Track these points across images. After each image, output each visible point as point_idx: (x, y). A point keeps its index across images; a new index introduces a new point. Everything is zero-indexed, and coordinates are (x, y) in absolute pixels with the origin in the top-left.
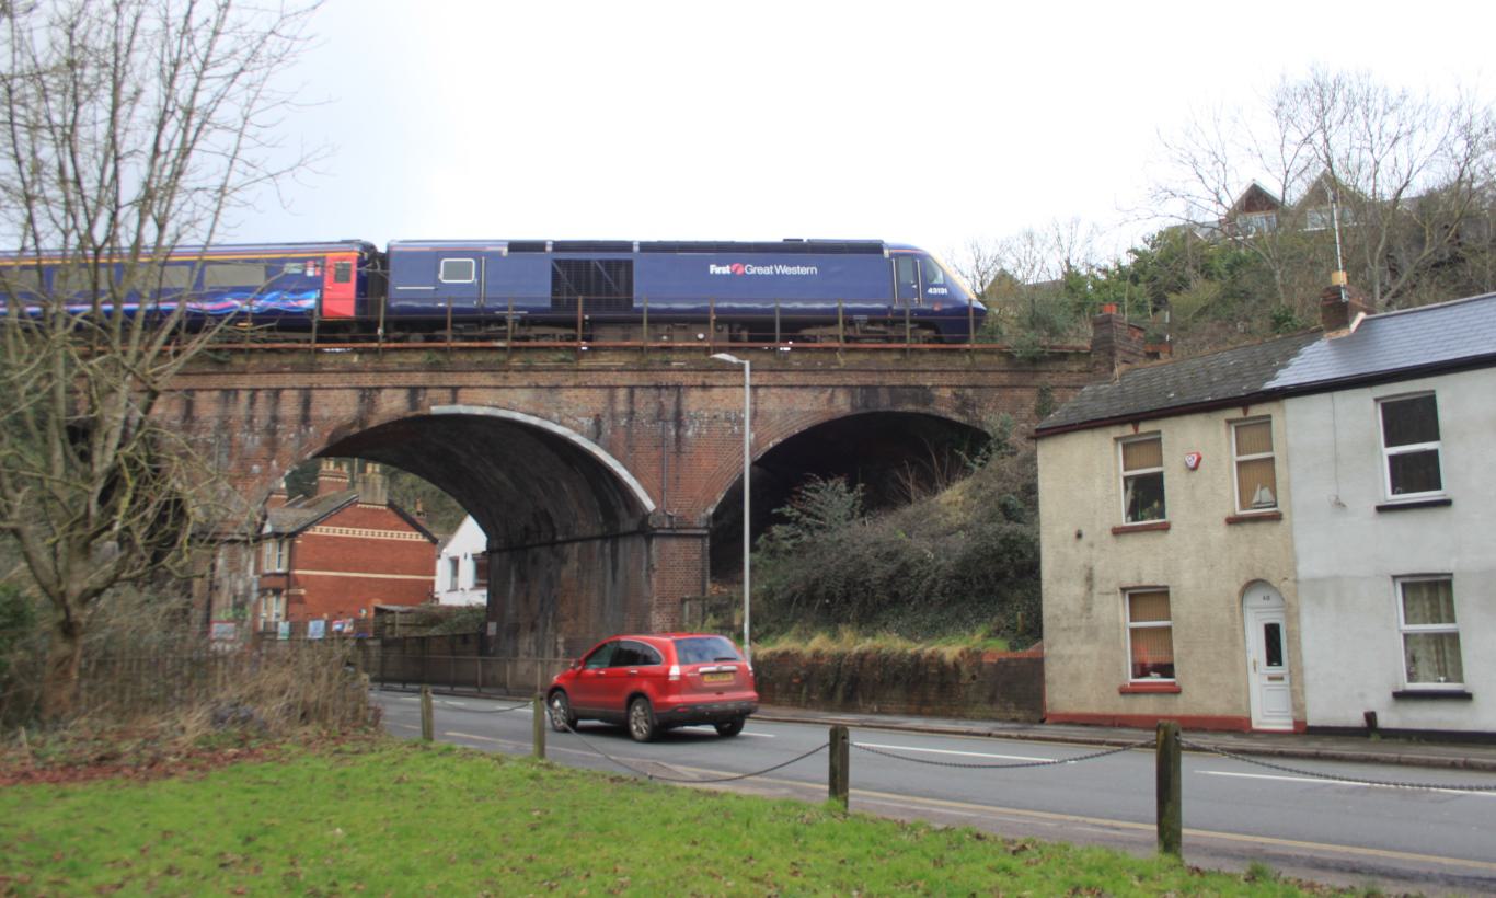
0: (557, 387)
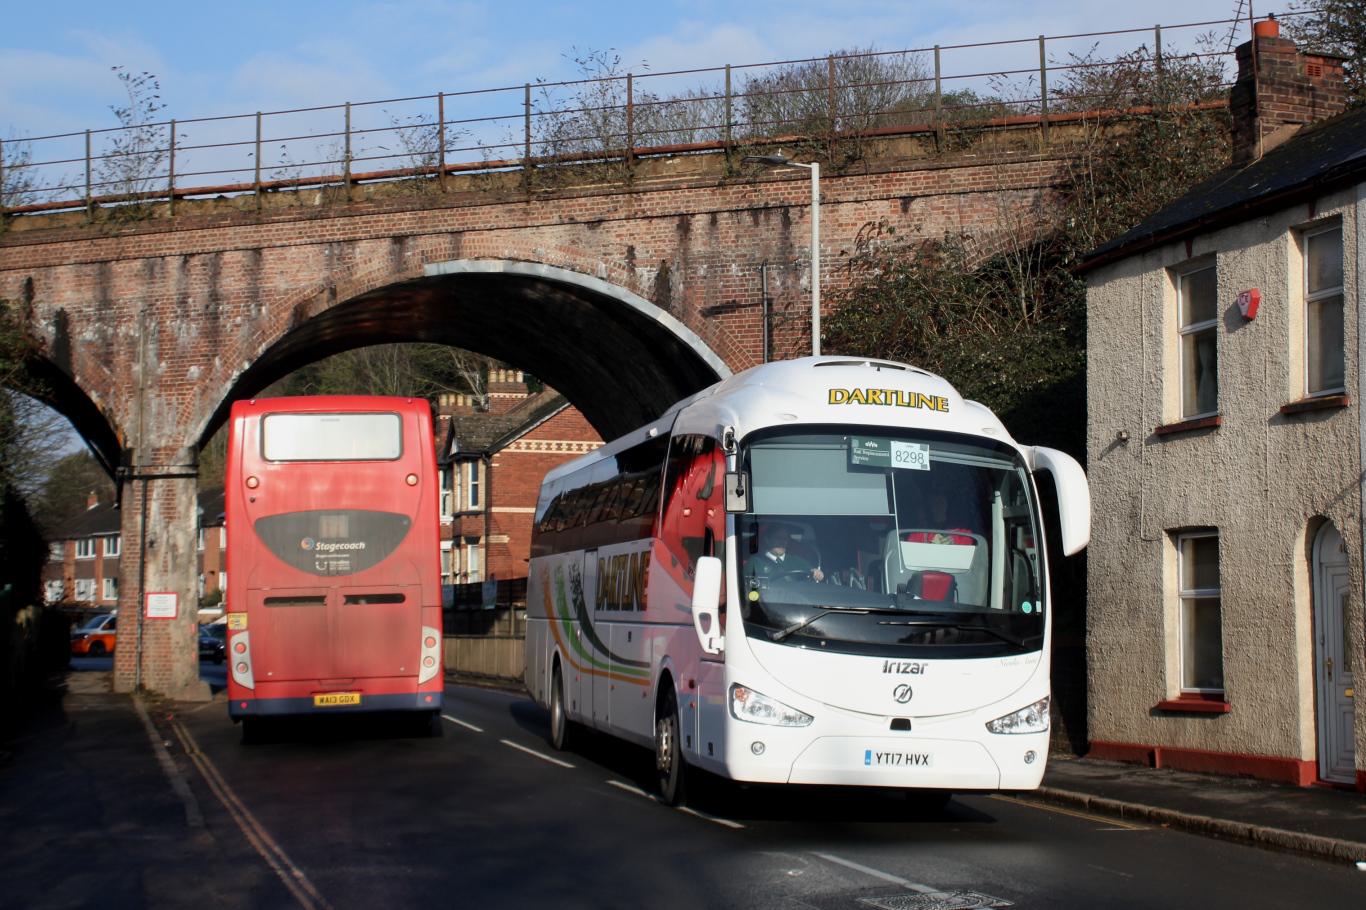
0: (600, 221)
